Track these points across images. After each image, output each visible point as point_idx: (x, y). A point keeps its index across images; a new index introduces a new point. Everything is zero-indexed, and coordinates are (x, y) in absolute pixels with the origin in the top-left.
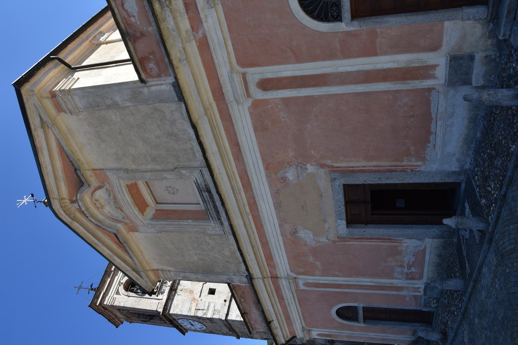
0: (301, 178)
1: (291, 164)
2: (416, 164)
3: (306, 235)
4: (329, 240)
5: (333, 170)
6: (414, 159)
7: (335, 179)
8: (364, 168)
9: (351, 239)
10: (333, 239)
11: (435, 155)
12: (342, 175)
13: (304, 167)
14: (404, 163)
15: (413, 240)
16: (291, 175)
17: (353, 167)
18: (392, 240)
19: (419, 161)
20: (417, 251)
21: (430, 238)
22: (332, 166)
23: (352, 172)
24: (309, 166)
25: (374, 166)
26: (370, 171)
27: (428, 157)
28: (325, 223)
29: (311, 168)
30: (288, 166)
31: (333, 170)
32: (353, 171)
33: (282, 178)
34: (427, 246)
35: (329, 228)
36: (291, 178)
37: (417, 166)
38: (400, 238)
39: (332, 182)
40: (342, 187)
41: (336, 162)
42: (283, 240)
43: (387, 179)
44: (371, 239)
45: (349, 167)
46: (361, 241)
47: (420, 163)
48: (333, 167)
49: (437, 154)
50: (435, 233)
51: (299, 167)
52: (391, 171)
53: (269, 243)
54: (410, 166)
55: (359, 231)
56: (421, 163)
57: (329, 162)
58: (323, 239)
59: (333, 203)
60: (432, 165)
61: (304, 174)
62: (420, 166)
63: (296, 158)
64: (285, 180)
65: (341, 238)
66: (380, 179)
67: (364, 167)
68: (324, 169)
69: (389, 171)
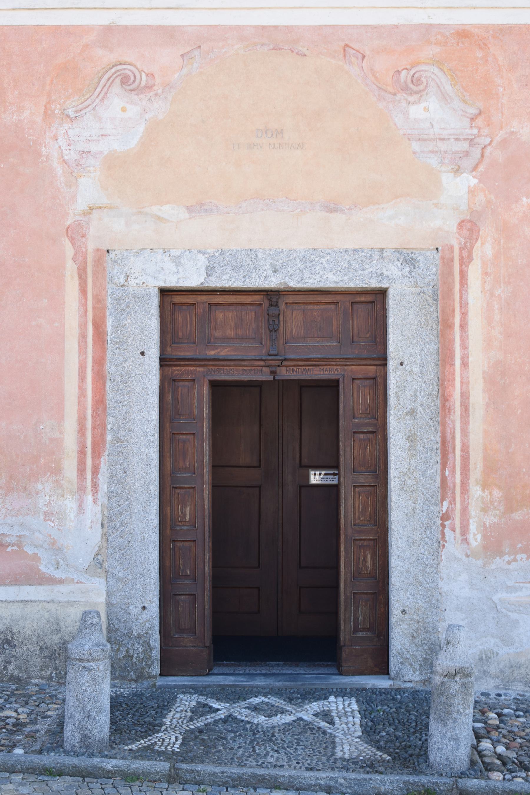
0: (416, 146)
1: (480, 121)
2: (473, 527)
3: (116, 123)
4: (85, 214)
5: (452, 266)
6: (491, 519)
7: (410, 261)
8: (458, 363)
9: (99, 301)
10: (92, 232)
11: (509, 583)
12: (429, 290)
13: (468, 163)
14: (476, 491)
15: (95, 536)
16: (434, 113)
17: (463, 326)
18: (97, 453)
19: (485, 537)
20: (29, 550)
21: (109, 594)
22: (470, 258)
23: (445, 326)
24: (469, 180)
25: (465, 396)
26: (443, 384)
27: (499, 562)
28: (189, 209)
29: (459, 188)
30: (472, 111)
31: (452, 266)
32: (445, 326)
33: (416, 81)
34: (63, 589)
35: (160, 219)
36: (416, 111)
37: (465, 531)
38: (103, 487)
39: (397, 250)
40: (374, 284)
41: (486, 274)
42: (85, 30)
43: (412, 438)
44: (100, 377)
45: (464, 315)
46: (83, 336)
47: (476, 539)
48: (466, 260)
49: (510, 589)
50: (134, 610)
51: (465, 146)
52: (445, 449)
53: (388, 365)
54: (465, 510)
55: (146, 329)
56: (474, 544)
57: (485, 249)
58: (88, 190)
59: (285, 240)
60: (464, 577)
61: (433, 161)
62: (466, 541)
63: (504, 143)
64: (405, 89)
65: (99, 262)
66: (412, 412)
67: (465, 365)
68: (455, 229)
69: (444, 442)
